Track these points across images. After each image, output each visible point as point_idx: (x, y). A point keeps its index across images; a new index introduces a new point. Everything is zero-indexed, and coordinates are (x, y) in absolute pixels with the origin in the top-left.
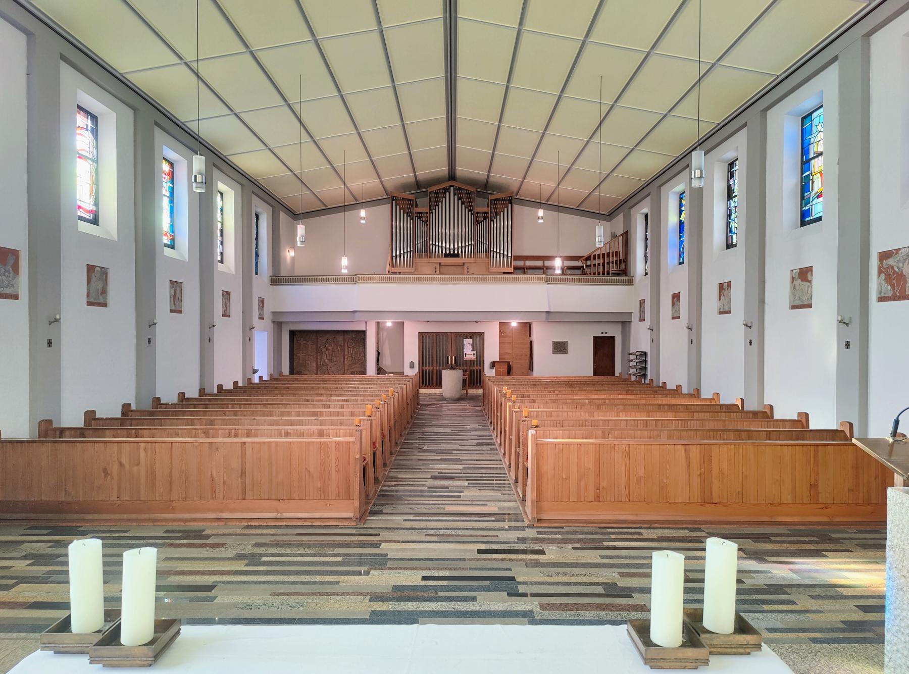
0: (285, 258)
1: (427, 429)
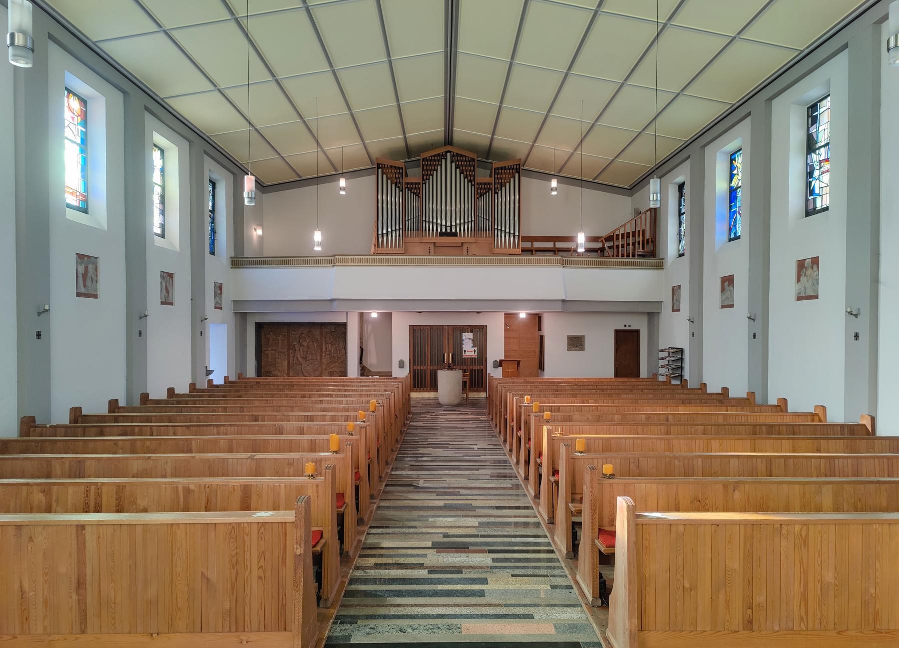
0: (251, 237)
1: (422, 451)
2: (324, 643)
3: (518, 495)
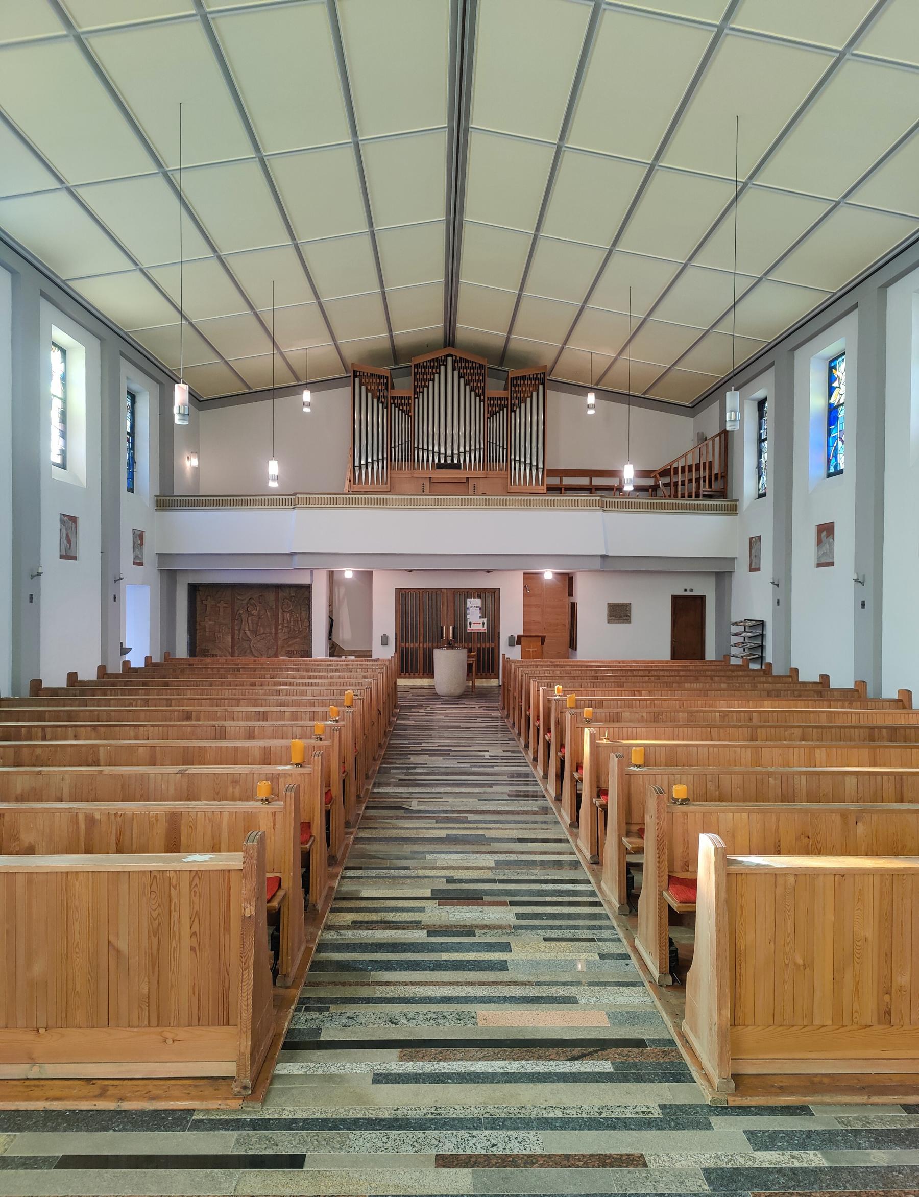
0: (182, 470)
1: (414, 759)
2: (282, 1039)
3: (545, 822)
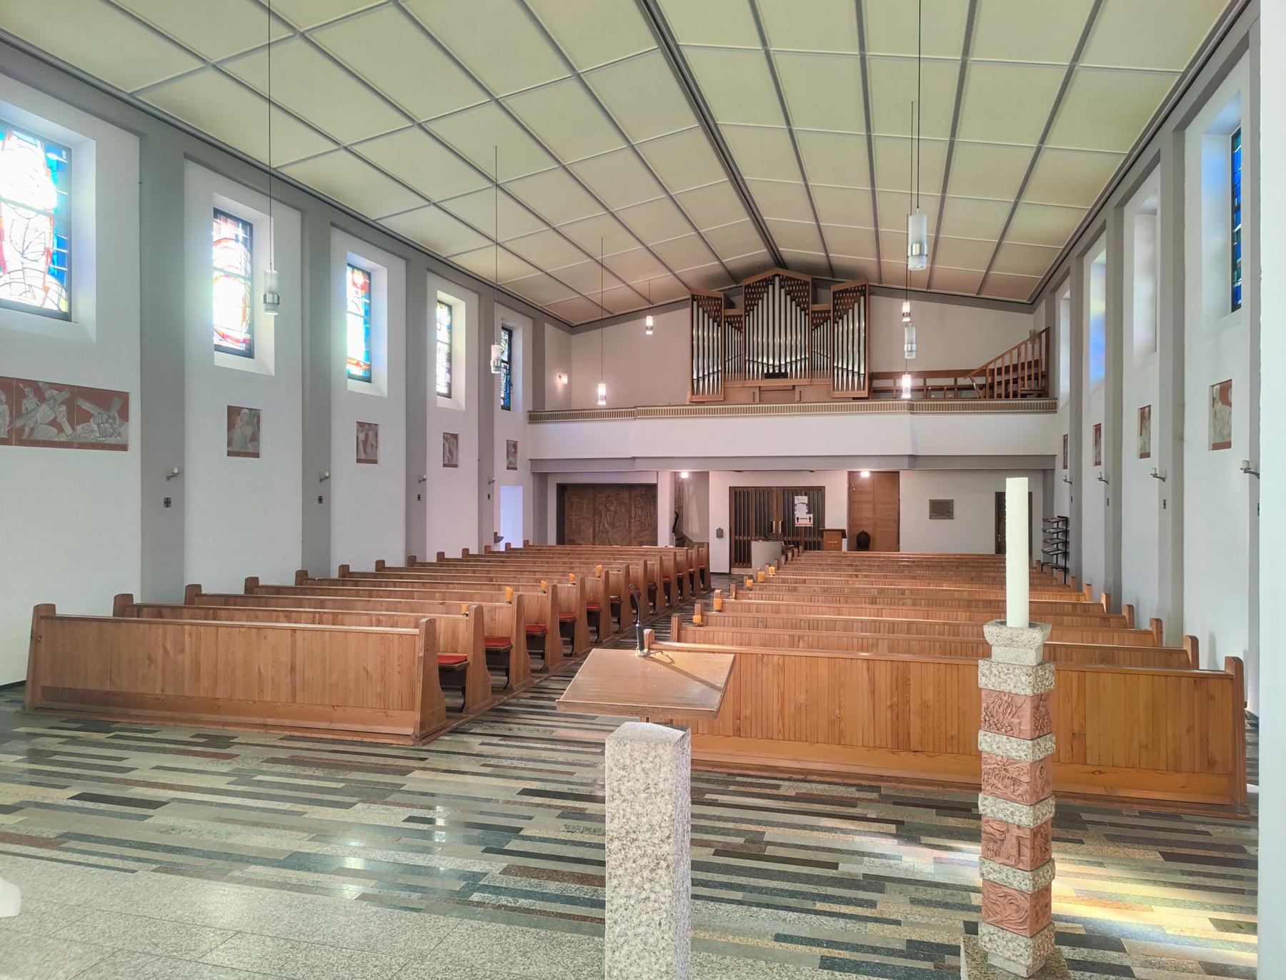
0: (554, 387)
